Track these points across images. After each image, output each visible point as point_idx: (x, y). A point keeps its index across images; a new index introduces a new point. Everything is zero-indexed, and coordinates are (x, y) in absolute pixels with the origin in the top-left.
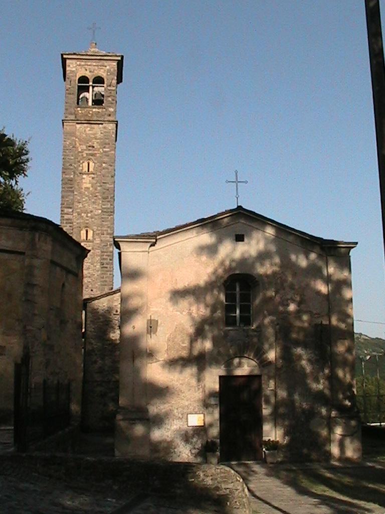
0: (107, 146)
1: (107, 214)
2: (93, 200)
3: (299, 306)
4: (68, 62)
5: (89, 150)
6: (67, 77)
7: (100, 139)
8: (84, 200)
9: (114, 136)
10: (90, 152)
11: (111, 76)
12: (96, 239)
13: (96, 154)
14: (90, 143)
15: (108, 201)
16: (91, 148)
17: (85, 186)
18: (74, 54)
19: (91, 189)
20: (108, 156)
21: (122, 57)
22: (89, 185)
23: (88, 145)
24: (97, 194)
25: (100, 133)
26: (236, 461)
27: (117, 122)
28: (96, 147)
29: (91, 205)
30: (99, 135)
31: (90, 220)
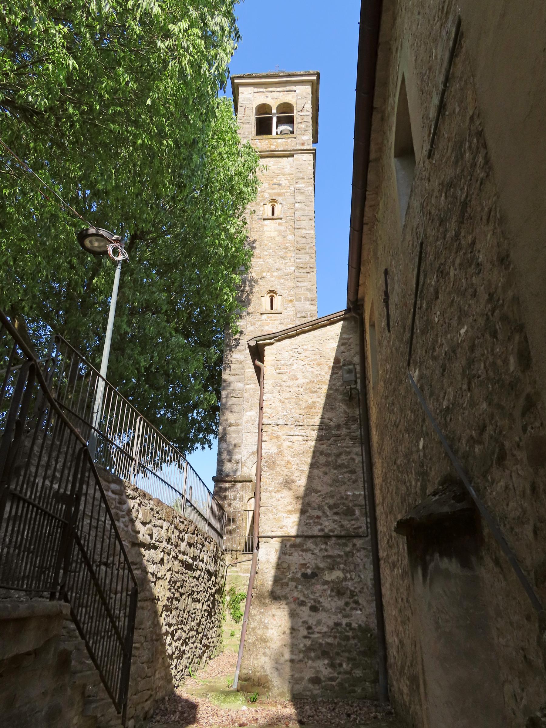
0: (300, 181)
1: (304, 271)
2: (281, 253)
3: (290, 489)
4: (241, 89)
5: (273, 189)
6: (239, 105)
7: (290, 174)
8: (266, 253)
9: (311, 168)
10: (275, 191)
11: (303, 101)
12: (288, 309)
13: (284, 193)
14: (275, 180)
15: (306, 253)
16: (276, 186)
17: (268, 234)
18: (250, 76)
19: (277, 238)
20: (302, 193)
21: (318, 75)
22: (275, 234)
23: (272, 182)
24: (287, 245)
25: (289, 168)
26: (18, 327)
27: (315, 150)
28: (283, 185)
29: (277, 261)
30: (287, 170)
31: (276, 281)
